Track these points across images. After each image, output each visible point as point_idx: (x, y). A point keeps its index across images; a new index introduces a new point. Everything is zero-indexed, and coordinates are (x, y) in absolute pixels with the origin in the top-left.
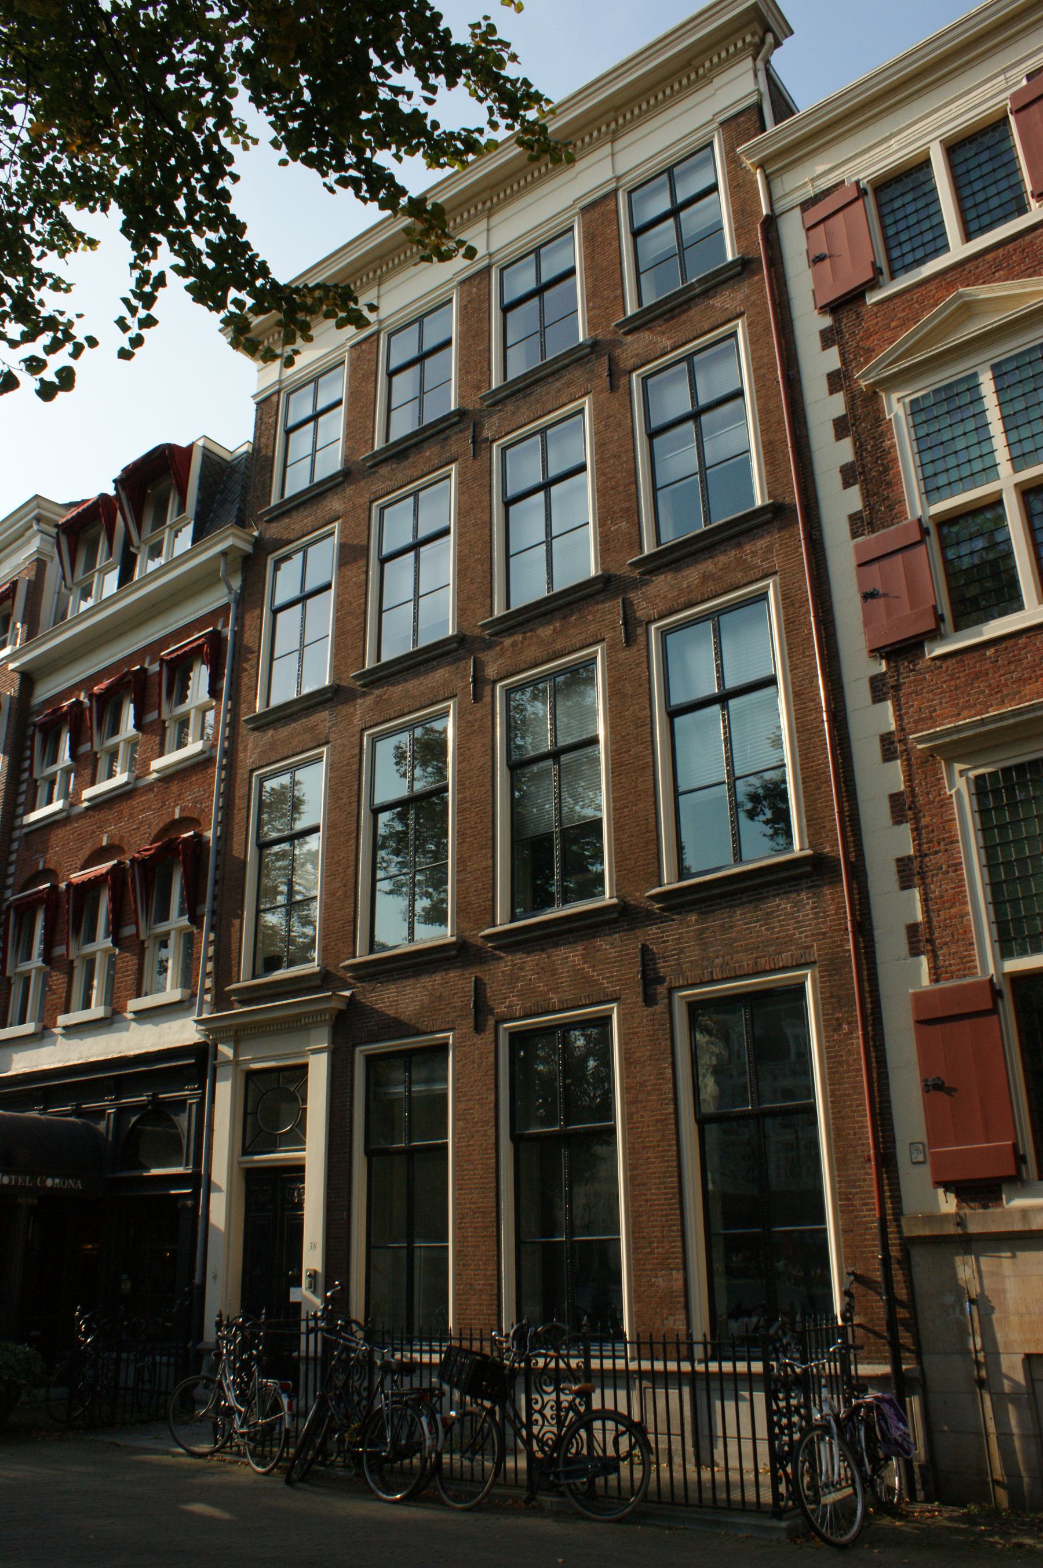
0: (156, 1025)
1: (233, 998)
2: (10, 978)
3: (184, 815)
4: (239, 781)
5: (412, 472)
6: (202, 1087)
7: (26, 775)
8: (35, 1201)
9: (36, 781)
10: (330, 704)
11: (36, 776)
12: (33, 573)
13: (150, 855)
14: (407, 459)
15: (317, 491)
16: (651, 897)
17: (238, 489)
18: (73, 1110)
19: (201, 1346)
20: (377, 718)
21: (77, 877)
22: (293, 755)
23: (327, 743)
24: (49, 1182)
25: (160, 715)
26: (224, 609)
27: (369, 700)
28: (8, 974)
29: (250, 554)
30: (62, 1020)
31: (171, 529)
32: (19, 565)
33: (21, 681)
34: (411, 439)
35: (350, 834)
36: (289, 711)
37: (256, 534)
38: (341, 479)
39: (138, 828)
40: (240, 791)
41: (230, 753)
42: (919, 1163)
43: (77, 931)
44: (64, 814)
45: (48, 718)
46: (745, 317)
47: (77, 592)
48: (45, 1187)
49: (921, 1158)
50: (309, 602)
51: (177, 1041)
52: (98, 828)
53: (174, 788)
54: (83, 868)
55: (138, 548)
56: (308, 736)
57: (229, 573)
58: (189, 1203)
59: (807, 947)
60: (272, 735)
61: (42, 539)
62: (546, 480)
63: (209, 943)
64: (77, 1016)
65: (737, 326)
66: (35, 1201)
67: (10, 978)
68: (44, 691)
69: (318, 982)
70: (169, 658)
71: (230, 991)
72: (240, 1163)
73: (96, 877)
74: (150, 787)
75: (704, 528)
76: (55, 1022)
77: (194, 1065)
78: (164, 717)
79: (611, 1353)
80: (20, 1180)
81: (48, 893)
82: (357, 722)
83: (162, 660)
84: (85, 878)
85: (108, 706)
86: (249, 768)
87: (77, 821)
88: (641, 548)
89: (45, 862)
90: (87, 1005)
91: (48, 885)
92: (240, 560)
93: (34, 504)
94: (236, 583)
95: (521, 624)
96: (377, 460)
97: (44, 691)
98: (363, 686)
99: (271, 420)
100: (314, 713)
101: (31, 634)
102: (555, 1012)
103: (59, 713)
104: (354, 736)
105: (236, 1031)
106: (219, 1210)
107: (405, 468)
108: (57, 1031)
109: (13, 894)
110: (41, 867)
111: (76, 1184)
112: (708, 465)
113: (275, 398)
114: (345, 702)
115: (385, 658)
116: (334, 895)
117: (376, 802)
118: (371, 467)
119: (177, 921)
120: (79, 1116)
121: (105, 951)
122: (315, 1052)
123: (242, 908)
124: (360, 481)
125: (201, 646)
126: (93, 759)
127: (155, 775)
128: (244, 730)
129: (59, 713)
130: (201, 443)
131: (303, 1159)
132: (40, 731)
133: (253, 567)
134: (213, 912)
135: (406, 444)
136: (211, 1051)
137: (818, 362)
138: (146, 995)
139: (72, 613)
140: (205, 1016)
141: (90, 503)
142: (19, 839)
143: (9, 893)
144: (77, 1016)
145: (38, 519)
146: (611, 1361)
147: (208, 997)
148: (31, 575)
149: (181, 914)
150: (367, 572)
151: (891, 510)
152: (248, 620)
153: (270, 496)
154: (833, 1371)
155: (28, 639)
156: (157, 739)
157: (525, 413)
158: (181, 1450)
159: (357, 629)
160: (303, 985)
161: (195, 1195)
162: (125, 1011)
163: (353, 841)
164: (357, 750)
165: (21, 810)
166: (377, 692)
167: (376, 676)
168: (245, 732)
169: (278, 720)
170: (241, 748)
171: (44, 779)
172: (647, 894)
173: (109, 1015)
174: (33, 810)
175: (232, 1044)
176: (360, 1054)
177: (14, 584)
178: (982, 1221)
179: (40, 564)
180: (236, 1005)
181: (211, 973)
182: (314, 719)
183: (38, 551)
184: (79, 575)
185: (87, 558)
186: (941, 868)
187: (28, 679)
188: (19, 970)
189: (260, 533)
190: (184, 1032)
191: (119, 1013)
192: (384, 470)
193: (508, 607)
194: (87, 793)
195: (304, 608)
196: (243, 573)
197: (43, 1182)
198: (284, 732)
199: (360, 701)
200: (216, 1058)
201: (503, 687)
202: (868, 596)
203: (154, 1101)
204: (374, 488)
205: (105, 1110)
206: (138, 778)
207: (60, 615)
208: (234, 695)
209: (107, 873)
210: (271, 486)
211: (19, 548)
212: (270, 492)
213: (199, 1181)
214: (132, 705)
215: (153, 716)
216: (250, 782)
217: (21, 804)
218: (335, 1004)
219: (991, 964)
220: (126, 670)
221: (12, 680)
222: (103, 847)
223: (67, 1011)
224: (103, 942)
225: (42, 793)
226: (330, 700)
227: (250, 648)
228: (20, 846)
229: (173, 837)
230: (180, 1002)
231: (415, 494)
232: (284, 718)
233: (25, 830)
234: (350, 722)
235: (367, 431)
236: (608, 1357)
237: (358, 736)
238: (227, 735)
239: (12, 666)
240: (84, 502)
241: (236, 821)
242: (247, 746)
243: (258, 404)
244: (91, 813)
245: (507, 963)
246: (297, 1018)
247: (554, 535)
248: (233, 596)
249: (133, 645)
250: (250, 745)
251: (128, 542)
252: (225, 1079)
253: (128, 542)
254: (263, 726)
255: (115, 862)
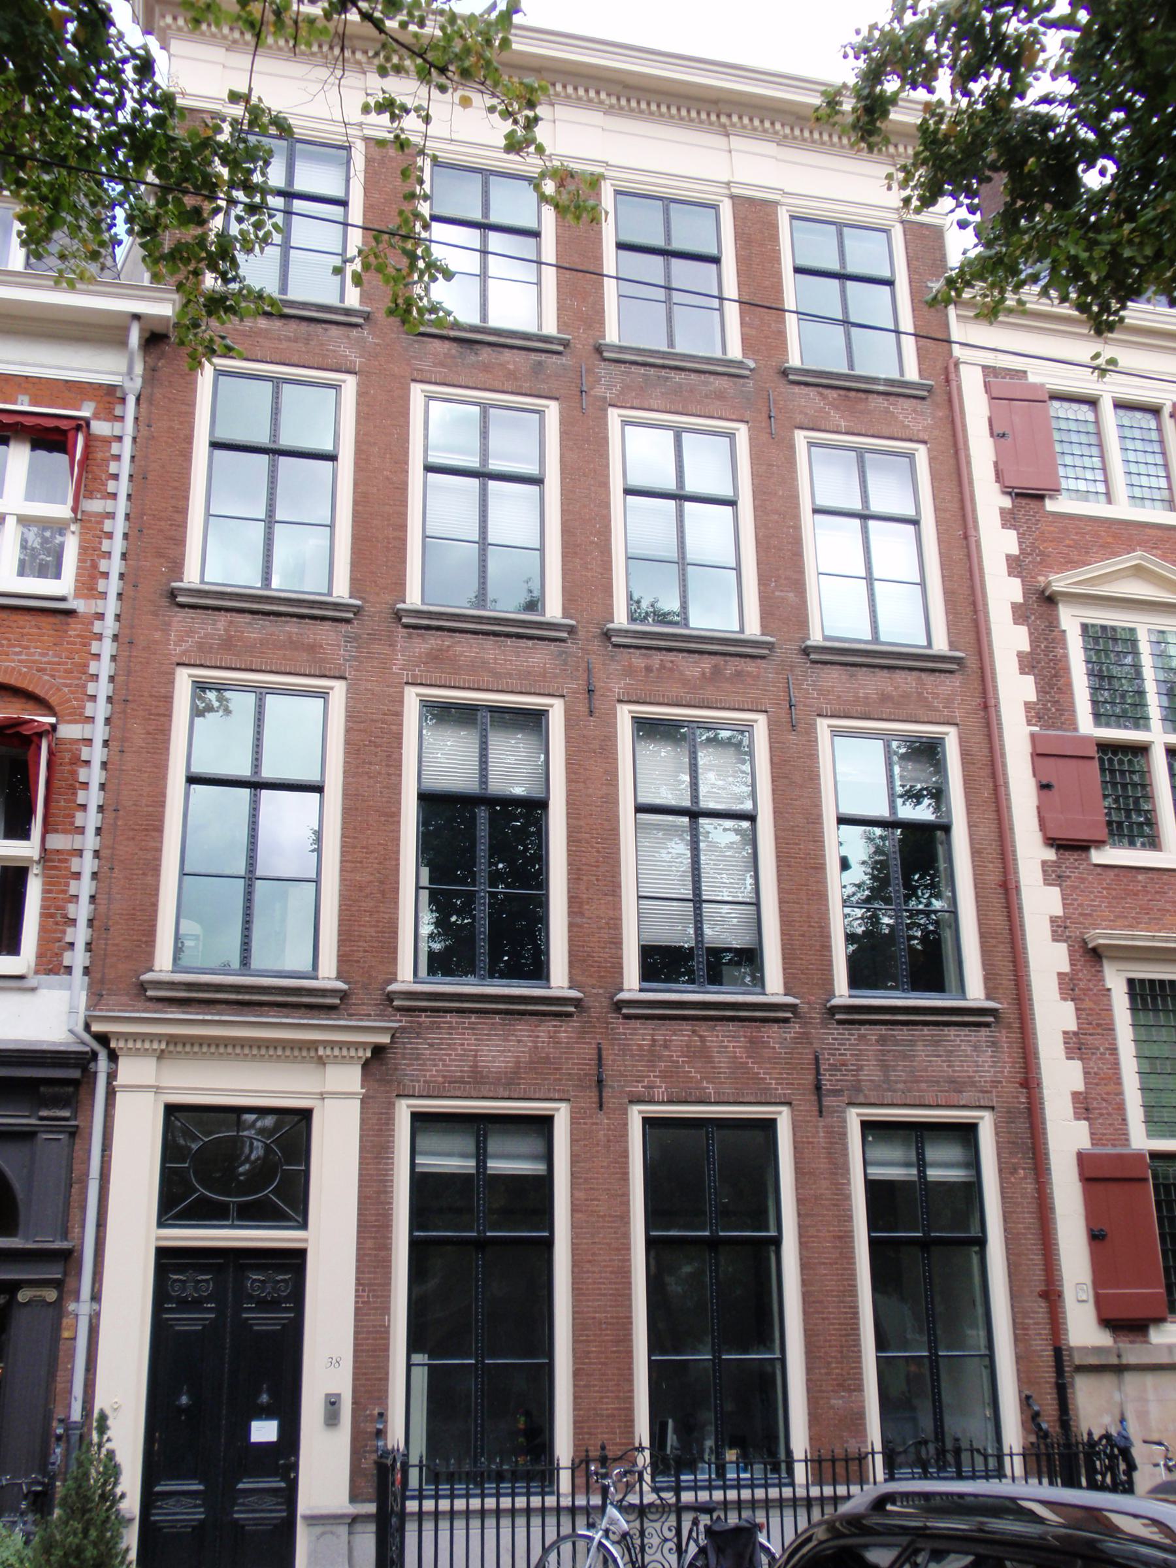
42: (1083, 1301)
49: (1084, 1298)
59: (987, 1092)
79: (539, 1490)
102: (710, 1103)
137: (997, 543)
146: (448, 1501)
151: (1061, 715)
176: (403, 1112)
178: (1134, 1354)
186: (1098, 1049)
202: (1044, 787)
219: (1141, 1140)
220: (85, 413)
236: (444, 1497)
245: (642, 1035)
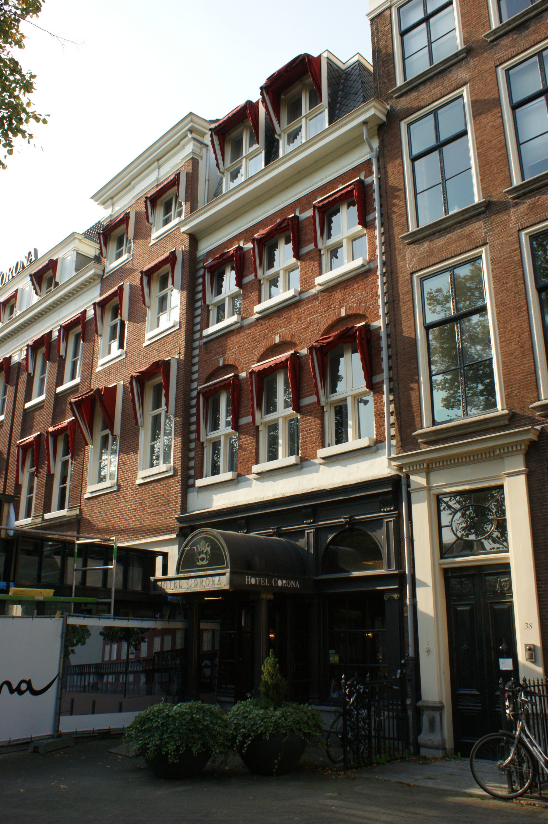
0: (345, 466)
1: (419, 441)
2: (203, 443)
3: (350, 312)
4: (400, 282)
5: (534, 38)
6: (398, 508)
7: (199, 304)
8: (272, 597)
9: (208, 306)
10: (482, 216)
11: (208, 302)
12: (191, 168)
13: (328, 343)
14: (528, 28)
15: (443, 67)
16: (534, 408)
17: (359, 85)
18: (274, 532)
19: (419, 704)
20: (532, 220)
21: (256, 367)
22: (452, 257)
23: (485, 244)
24: (280, 583)
25: (256, 276)
26: (366, 165)
27: (523, 208)
28: (202, 440)
29: (385, 123)
30: (256, 468)
31: (306, 118)
32: (177, 164)
33: (189, 242)
34: (531, 12)
35: (520, 308)
36: (444, 226)
37: (388, 107)
38: (464, 55)
39: (308, 327)
40: (402, 289)
41: (390, 265)
43: (259, 407)
44: (238, 325)
45: (216, 262)
46: (468, 85)
47: (228, 175)
48: (278, 586)
50: (445, 149)
51: (251, 500)
52: (269, 331)
53: (338, 295)
54: (259, 361)
55: (280, 135)
56: (465, 242)
57: (370, 137)
58: (396, 596)
60: (429, 246)
61: (194, 144)
62: (439, 143)
63: (390, 402)
64: (265, 466)
65: (463, 91)
66: (272, 597)
67: (203, 443)
68: (206, 246)
69: (507, 422)
70: (321, 204)
71: (418, 435)
72: (440, 564)
73: (276, 364)
74: (315, 297)
75: (444, 217)
76: (251, 469)
77: (391, 493)
78: (260, 277)
80: (262, 581)
81: (233, 380)
82: (513, 225)
83: (314, 207)
84: (261, 368)
85: (267, 246)
86: (409, 272)
87: (249, 329)
88: (408, 228)
89: (224, 360)
90: (273, 456)
91: (232, 374)
92: (376, 128)
93: (189, 119)
94: (376, 144)
95: (428, 236)
96: (498, 35)
97: (206, 246)
98: (514, 198)
99: (386, 29)
100: (468, 224)
101: (193, 209)
103: (225, 257)
104: (511, 236)
105: (428, 465)
106: (427, 600)
107: (527, 36)
108: (318, 461)
109: (199, 385)
110: (221, 364)
111: (296, 584)
112: (521, 142)
113: (387, 13)
114: (498, 212)
115: (422, 225)
116: (512, 355)
117: (427, 322)
118: (492, 41)
119: (283, 411)
120: (280, 536)
121: (226, 436)
122: (510, 475)
123: (418, 374)
124: (482, 53)
125: (352, 191)
126: (258, 285)
127: (318, 288)
128: (399, 245)
129: (225, 257)
130: (325, 55)
131: (508, 558)
132: (208, 272)
133: (386, 131)
134: (390, 380)
135: (526, 18)
136: (403, 481)
138: (329, 446)
139: (226, 190)
140: (393, 456)
141: (221, 122)
142: (199, 347)
143: (195, 385)
144: (265, 466)
145: (191, 131)
147: (394, 442)
148: (190, 169)
149: (286, 406)
150: (502, 117)
152: (390, 168)
153: (395, 80)
154: (535, 711)
155: (191, 212)
156: (316, 264)
157: (523, 43)
158: (482, 792)
159: (500, 158)
160: (491, 425)
161: (402, 591)
162: (315, 457)
163: (525, 313)
164: (517, 246)
165: (198, 327)
166: (529, 201)
167: (528, 189)
168: (401, 247)
169: (433, 234)
170: (399, 258)
171: (214, 305)
172: (531, 406)
173: (299, 462)
174: (208, 326)
175: (424, 474)
177: (178, 175)
179: (194, 162)
180: (422, 445)
181: (394, 424)
182: (468, 229)
183: (193, 152)
184: (228, 163)
185: (288, 118)
187: (194, 239)
188: (209, 437)
189: (391, 107)
190: (379, 467)
191: (307, 460)
192: (505, 41)
193: (418, 226)
194: (258, 308)
195: (441, 154)
196: (379, 136)
197: (276, 582)
198: (440, 242)
199: (512, 210)
200: (409, 486)
201: (418, 277)
203: (352, 523)
204: (497, 56)
205: (304, 531)
206: (301, 292)
207: (216, 193)
208: (387, 222)
209: (287, 360)
210: (395, 73)
211: (176, 154)
212: (395, 77)
213: (404, 580)
214: (233, 272)
215: (250, 278)
216: (412, 282)
217: (198, 323)
218: (532, 436)
221: (182, 240)
222: (277, 344)
223: (257, 462)
224: (224, 429)
225: (213, 314)
226: (483, 212)
227: (396, 187)
228: (200, 352)
229: (349, 326)
230: (231, 480)
231: (435, 112)
232: (439, 231)
233: (205, 340)
234: (506, 226)
235: (483, 17)
237: (516, 235)
238: (383, 251)
239: (183, 229)
240: (218, 120)
241: (403, 311)
242: (404, 256)
243: (372, 20)
244: (261, 322)
246: (493, 449)
247: (447, 178)
248: (374, 153)
249: (283, 203)
250: (408, 256)
251: (270, 131)
252: (420, 501)
253: (270, 131)
254: (418, 240)
255: (292, 352)
